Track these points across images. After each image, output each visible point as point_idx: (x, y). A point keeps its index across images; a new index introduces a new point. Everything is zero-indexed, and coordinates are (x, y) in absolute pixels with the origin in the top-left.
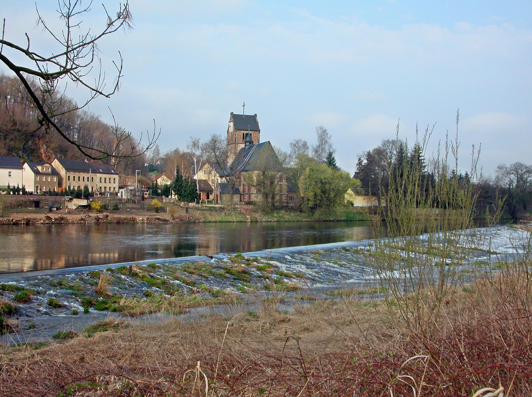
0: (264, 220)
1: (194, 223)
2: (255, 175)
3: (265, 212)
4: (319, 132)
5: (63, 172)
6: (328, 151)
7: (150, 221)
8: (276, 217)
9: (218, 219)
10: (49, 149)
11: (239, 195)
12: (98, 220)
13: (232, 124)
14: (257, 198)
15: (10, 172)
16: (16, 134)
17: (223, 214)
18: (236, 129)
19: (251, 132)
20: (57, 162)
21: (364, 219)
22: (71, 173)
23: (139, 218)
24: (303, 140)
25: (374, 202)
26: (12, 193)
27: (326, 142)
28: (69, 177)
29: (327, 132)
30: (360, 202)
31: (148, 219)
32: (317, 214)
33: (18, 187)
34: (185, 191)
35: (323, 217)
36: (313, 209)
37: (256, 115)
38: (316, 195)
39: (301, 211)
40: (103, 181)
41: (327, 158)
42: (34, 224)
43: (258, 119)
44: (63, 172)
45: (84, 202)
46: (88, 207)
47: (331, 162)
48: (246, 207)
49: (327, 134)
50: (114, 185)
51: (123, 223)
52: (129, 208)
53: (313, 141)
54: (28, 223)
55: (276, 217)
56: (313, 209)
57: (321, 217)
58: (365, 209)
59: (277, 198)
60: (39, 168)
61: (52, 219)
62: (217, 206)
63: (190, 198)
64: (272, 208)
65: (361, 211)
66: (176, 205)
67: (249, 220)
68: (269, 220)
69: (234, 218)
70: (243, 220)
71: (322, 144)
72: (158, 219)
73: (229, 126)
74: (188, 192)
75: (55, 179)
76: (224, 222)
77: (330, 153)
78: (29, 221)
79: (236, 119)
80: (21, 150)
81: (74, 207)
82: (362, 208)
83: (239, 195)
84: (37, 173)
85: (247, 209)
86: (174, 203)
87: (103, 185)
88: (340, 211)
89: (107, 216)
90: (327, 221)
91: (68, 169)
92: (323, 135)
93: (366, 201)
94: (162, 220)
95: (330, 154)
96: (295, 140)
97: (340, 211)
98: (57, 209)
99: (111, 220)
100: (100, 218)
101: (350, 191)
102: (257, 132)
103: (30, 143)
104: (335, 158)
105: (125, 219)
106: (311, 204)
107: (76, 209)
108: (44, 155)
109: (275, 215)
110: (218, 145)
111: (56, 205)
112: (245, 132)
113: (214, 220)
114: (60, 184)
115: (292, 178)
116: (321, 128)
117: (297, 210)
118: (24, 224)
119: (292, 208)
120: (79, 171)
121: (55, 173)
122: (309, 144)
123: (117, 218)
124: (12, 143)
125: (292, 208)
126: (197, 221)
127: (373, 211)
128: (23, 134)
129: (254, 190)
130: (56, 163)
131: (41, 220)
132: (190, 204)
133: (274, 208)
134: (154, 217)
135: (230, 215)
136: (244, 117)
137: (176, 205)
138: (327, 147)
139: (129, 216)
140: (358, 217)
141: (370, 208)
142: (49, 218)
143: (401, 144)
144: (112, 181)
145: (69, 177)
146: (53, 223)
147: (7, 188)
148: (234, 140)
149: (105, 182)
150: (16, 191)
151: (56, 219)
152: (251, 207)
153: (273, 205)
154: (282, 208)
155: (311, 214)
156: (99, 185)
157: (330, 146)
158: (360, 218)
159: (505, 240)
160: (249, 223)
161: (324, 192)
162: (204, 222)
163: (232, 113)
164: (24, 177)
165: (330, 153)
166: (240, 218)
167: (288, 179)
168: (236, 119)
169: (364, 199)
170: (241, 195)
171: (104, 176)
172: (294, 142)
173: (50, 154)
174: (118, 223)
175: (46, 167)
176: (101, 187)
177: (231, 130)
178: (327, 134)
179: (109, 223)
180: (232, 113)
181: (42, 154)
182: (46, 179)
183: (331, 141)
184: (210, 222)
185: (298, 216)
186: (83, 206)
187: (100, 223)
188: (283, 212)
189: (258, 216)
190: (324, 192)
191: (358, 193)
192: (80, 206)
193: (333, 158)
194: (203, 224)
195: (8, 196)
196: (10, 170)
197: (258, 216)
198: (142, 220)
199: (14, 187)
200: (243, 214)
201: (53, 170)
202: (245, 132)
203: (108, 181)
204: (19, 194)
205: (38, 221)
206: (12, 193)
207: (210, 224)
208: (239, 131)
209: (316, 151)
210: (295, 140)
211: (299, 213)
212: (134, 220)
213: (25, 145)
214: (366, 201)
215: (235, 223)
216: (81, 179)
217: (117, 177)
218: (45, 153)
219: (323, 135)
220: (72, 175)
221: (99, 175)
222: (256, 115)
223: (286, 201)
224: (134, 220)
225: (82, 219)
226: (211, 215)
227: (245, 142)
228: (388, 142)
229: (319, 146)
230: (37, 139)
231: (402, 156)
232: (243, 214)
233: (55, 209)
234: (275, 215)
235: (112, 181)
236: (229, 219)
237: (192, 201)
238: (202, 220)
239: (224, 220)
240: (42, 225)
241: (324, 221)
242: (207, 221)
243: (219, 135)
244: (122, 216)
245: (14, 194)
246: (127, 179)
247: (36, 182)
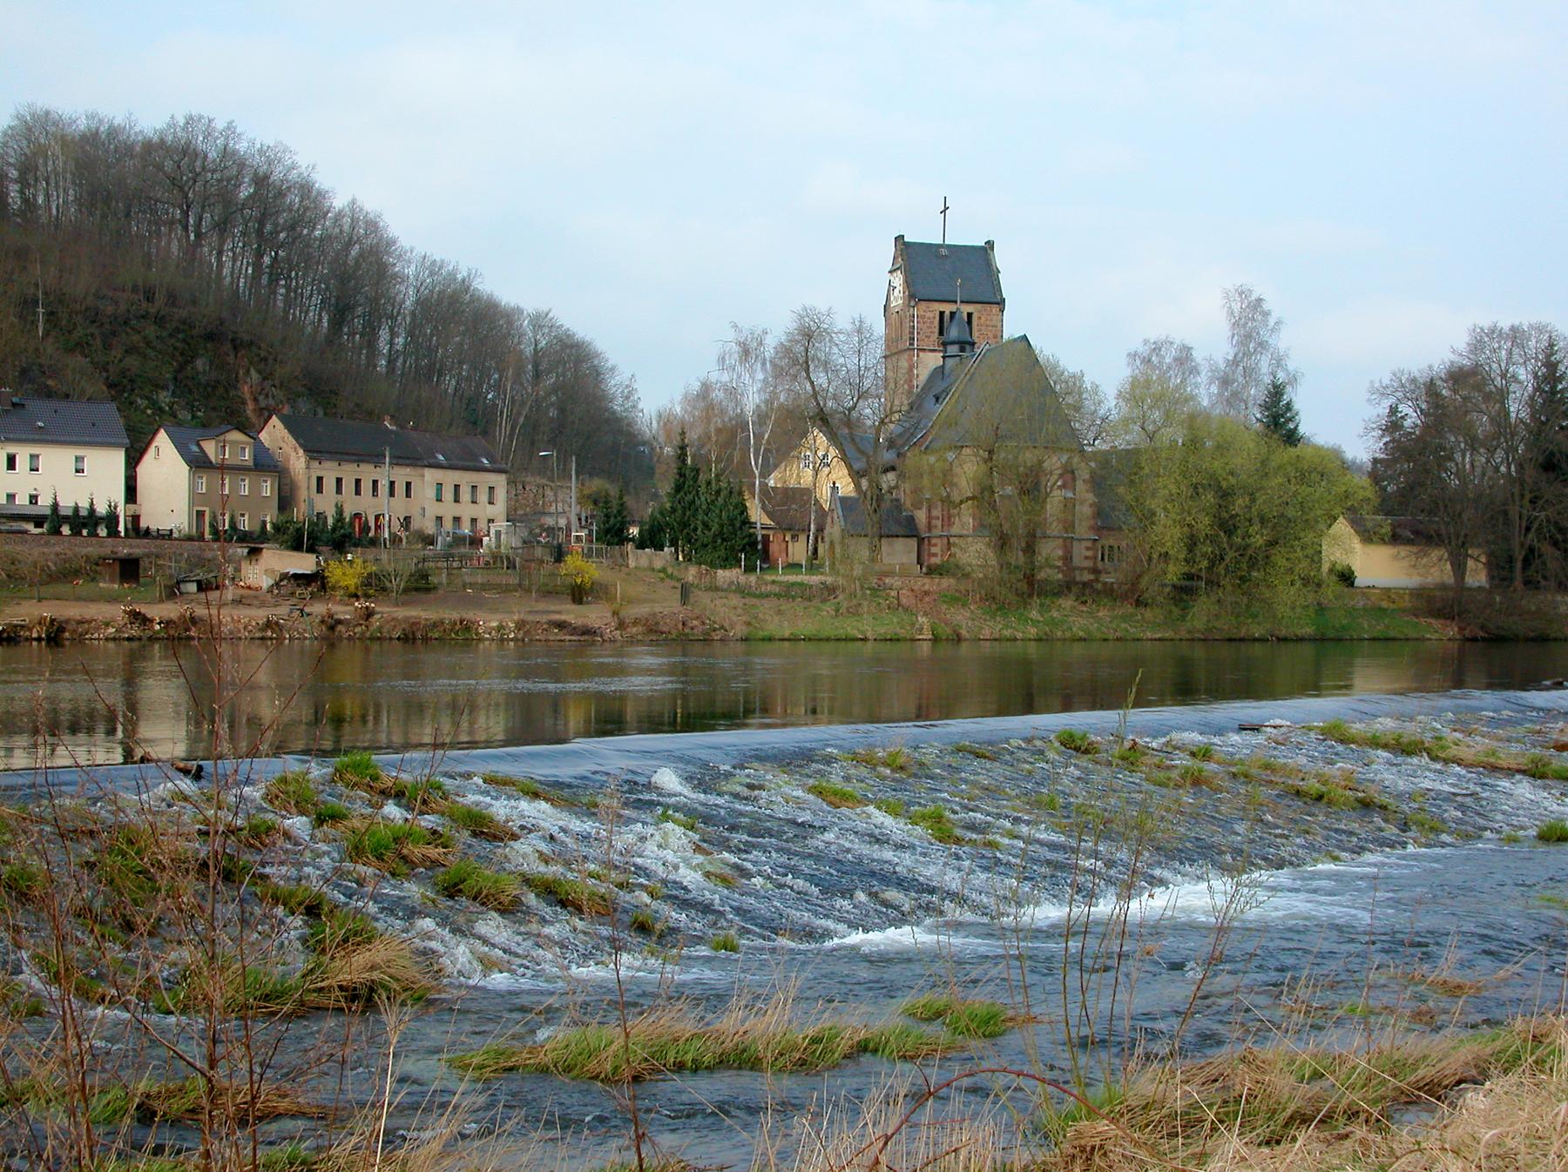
0: (986, 633)
1: (707, 640)
2: (968, 470)
3: (994, 603)
4: (1236, 307)
5: (297, 461)
6: (1267, 380)
7: (527, 633)
8: (1035, 623)
9: (806, 627)
10: (268, 384)
11: (913, 543)
12: (332, 628)
13: (898, 280)
14: (975, 553)
15: (79, 459)
16: (151, 331)
17: (829, 608)
18: (912, 296)
19: (966, 309)
20: (279, 425)
21: (1392, 634)
22: (328, 464)
23: (487, 622)
24: (1178, 342)
25: (1434, 570)
26: (66, 530)
27: (1262, 345)
28: (320, 480)
29: (1266, 306)
30: (1379, 567)
31: (520, 625)
32: (1202, 613)
33: (92, 510)
34: (706, 526)
35: (1225, 625)
36: (1184, 592)
37: (990, 244)
38: (1192, 543)
39: (1138, 603)
40: (448, 495)
41: (1266, 407)
42: (79, 640)
43: (1000, 258)
44: (297, 461)
45: (304, 563)
46: (315, 582)
47: (1279, 419)
48: (927, 584)
49: (1266, 314)
50: (491, 511)
51: (426, 639)
52: (471, 585)
53: (1212, 343)
54: (55, 635)
55: (1035, 623)
56: (1184, 592)
57: (1218, 624)
58: (1401, 597)
59: (1050, 550)
60: (210, 448)
61: (151, 621)
62: (815, 579)
63: (722, 553)
64: (1024, 586)
65: (1384, 604)
66: (671, 576)
67: (927, 635)
68: (1007, 633)
69: (866, 626)
70: (902, 633)
71: (1248, 354)
72: (561, 625)
73: (891, 288)
74: (715, 528)
75: (268, 488)
76: (828, 639)
77: (1275, 386)
78: (61, 630)
79: (915, 259)
80: (165, 388)
81: (266, 582)
82: (1387, 591)
83: (913, 543)
84: (198, 463)
85: (926, 593)
86: (664, 570)
87: (448, 509)
88: (1288, 604)
89: (369, 614)
90: (1242, 640)
91: (315, 452)
92: (1250, 323)
93: (1405, 563)
94: (574, 630)
95: (1277, 392)
96: (1146, 342)
97: (1288, 604)
98: (200, 589)
99: (380, 629)
100: (339, 622)
101: (1342, 527)
102: (995, 308)
103: (200, 364)
104: (1296, 406)
105: (435, 625)
106: (1174, 572)
107: (270, 591)
108: (250, 406)
109: (1034, 614)
110: (820, 349)
111: (202, 575)
112: (948, 308)
113: (787, 634)
114: (285, 501)
115: (1116, 476)
116: (1242, 293)
117: (1124, 597)
118: (39, 639)
119: (1109, 591)
120: (360, 458)
121: (265, 464)
122: (1198, 355)
123: (406, 619)
124: (132, 362)
125: (1109, 591)
126: (717, 636)
127: (1432, 604)
128: (177, 330)
129: (966, 520)
130: (275, 434)
131: (107, 625)
132: (720, 572)
133: (1031, 588)
134: (545, 618)
135: (854, 612)
136: (943, 251)
137: (671, 576)
138: (1264, 365)
139: (450, 614)
140: (1367, 627)
141: (1418, 593)
142: (137, 617)
143: (1551, 345)
144: (483, 497)
145: (320, 480)
146: (153, 639)
147: (48, 512)
148: (906, 337)
149: (457, 500)
150: (85, 526)
151: (168, 623)
152: (947, 582)
153: (1030, 579)
154: (1066, 587)
155: (1176, 611)
156: (433, 510)
157: (1279, 362)
158: (1379, 630)
159: (3, 528)
160: (926, 647)
161: (1227, 526)
162: (745, 640)
163: (899, 239)
164: (78, 477)
165: (1275, 386)
166: (891, 624)
167: (1097, 483)
168: (915, 259)
169: (1396, 557)
170: (921, 541)
171: (450, 478)
172: (1143, 350)
173: (271, 402)
174: (408, 638)
175: (232, 443)
176: (439, 519)
177: (898, 300)
178: (1266, 314)
179: (372, 639)
180: (899, 239)
181: (244, 403)
182: (255, 489)
183: (1282, 341)
184: (770, 639)
185: (1124, 618)
186: (296, 577)
187: (340, 638)
188: (1067, 603)
189: (963, 618)
190: (1227, 526)
191: (1367, 537)
192: (284, 576)
193: (1289, 407)
194: (740, 647)
195: (53, 539)
196: (80, 452)
197: (963, 618)
198: (500, 628)
199: (76, 509)
200: (906, 609)
201: (261, 453)
202: (948, 308)
203: (465, 495)
204: (93, 534)
205: (97, 629)
206: (66, 530)
207: (767, 646)
208: (923, 305)
209: (1225, 382)
210: (1146, 342)
211: (1131, 609)
212: (468, 629)
213: (182, 368)
214: (1405, 563)
215: (870, 645)
216: (366, 486)
217: (500, 481)
218: (255, 400)
219: (1250, 323)
220: (329, 471)
221: (431, 475)
222: (990, 244)
223: (1089, 564)
224: (467, 626)
225: (269, 624)
226: (780, 612)
227: (945, 344)
228: (1494, 332)
229: (1235, 362)
230: (228, 347)
231: (1553, 392)
232: (906, 609)
233: (193, 587)
234: (1034, 614)
235: (483, 497)
236: (850, 628)
237: (729, 561)
238: (740, 630)
239: (828, 631)
240: (111, 645)
241: (1230, 640)
242: (761, 634)
243: (824, 310)
244: (424, 615)
245: (76, 532)
246: (549, 492)
247: (194, 496)
